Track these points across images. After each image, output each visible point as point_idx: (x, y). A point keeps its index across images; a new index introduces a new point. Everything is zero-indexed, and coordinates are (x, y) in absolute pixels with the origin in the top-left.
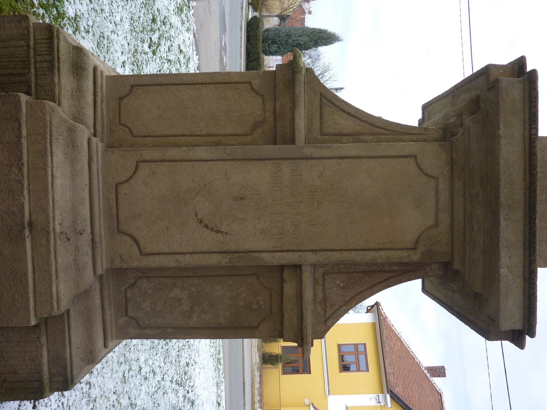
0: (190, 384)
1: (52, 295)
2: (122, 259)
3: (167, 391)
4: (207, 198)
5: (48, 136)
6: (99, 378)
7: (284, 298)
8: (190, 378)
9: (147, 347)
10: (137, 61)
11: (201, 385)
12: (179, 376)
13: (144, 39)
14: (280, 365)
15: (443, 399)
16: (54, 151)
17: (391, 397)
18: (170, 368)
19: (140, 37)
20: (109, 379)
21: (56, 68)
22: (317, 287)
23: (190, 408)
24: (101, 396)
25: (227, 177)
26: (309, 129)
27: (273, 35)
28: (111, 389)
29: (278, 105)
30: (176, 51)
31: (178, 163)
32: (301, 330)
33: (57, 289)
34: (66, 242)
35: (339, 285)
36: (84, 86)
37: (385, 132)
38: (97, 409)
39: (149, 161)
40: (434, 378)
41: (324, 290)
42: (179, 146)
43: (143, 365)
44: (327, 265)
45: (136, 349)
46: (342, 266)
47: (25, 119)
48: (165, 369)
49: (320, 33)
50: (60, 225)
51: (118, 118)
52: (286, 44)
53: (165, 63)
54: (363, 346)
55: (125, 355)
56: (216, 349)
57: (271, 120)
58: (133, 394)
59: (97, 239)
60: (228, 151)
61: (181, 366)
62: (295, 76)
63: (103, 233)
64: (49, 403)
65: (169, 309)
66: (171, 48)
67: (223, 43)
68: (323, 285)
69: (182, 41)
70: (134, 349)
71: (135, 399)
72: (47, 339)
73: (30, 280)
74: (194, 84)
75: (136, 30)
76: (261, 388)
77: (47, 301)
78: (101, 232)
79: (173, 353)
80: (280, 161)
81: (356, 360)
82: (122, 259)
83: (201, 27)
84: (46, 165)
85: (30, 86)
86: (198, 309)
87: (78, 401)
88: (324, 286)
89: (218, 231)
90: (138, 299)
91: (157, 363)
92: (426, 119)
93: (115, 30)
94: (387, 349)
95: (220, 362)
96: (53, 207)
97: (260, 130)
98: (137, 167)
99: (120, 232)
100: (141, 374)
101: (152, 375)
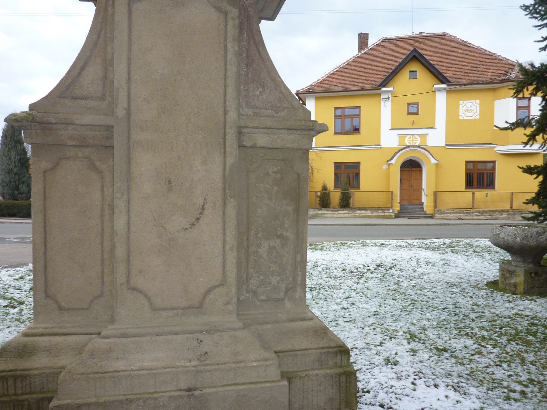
0: (362, 268)
1: (259, 366)
2: (228, 303)
3: (366, 286)
6: (348, 341)
7: (271, 147)
8: (356, 268)
9: (325, 304)
10: (29, 319)
11: (363, 258)
12: (353, 277)
14: (351, 191)
15: (388, 38)
16: (114, 369)
17: (384, 87)
20: (350, 333)
21: (23, 372)
22: (262, 115)
23: (383, 268)
24: (365, 339)
25: (146, 197)
27: (8, 189)
28: (359, 331)
29: (70, 142)
30: (20, 283)
34: (208, 356)
35: (261, 92)
38: (375, 342)
40: (369, 44)
42: (113, 249)
43: (341, 307)
45: (325, 313)
46: (242, 87)
47: (79, 400)
49: (6, 137)
50: (191, 361)
52: (19, 175)
54: (337, 110)
56: (333, 247)
57: (87, 151)
58: (365, 314)
61: (345, 275)
64: (366, 380)
66: (17, 287)
67: (16, 240)
69: (10, 278)
70: (325, 314)
71: (370, 312)
76: (371, 209)
79: (332, 282)
81: (350, 118)
82: (228, 303)
85: (43, 399)
87: (367, 357)
89: (203, 208)
90: (268, 288)
91: (340, 295)
94: (340, 87)
95: (345, 243)
96: (172, 368)
97: (98, 163)
98: (135, 289)
99: (201, 305)
100: (349, 308)
101: (350, 299)
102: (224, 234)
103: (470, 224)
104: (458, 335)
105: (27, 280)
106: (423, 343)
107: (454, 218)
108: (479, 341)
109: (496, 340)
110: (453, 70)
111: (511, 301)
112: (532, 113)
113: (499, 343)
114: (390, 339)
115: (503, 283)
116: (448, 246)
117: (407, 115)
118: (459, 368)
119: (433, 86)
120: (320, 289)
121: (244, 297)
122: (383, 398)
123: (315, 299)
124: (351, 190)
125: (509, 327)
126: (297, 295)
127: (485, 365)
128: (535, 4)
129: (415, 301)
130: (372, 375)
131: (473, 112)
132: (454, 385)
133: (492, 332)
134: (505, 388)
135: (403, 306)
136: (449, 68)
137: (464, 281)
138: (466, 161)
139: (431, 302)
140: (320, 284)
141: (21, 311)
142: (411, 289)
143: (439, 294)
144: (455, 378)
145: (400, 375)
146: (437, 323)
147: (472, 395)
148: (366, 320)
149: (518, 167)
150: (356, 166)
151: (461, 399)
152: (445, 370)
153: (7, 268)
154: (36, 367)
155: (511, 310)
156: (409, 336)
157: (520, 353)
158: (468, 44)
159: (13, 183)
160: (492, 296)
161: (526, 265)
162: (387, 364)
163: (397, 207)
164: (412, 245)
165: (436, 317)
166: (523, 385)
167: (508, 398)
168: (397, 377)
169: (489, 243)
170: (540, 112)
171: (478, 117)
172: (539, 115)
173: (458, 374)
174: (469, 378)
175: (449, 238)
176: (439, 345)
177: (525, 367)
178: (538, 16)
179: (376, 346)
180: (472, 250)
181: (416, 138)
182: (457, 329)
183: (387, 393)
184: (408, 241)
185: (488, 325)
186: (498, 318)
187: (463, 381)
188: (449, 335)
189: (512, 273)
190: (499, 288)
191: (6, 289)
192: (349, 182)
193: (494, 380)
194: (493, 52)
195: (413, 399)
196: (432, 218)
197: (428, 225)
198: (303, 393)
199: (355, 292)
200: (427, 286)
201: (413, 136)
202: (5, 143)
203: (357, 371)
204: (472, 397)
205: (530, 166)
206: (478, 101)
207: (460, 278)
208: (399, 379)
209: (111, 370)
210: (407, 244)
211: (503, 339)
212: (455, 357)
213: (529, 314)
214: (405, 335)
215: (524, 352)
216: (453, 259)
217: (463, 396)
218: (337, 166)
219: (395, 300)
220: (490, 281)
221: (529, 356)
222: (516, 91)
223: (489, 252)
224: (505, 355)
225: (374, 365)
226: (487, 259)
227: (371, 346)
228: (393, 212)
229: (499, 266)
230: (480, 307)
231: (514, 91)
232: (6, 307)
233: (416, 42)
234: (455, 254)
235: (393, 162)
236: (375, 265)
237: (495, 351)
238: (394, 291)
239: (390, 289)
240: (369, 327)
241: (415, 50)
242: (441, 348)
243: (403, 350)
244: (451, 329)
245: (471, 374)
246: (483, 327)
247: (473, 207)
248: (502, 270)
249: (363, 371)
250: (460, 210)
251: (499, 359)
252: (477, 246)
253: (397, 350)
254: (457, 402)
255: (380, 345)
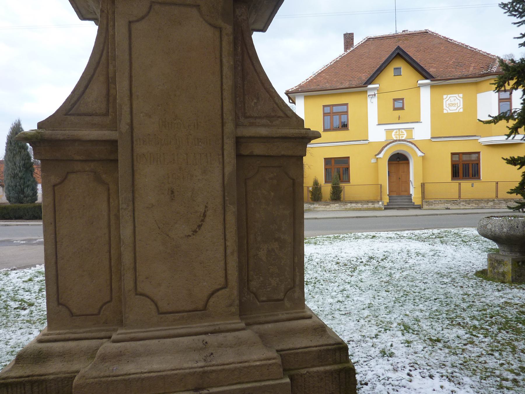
0: (355, 261)
2: (231, 305)
3: (360, 279)
4: (172, 226)
5: (110, 379)
6: (345, 334)
7: (266, 154)
9: (321, 297)
10: (40, 320)
11: (356, 251)
12: (347, 270)
13: (16, 315)
14: (342, 185)
15: (372, 37)
16: (125, 372)
17: (370, 84)
18: (340, 278)
19: (13, 319)
20: (346, 326)
21: (39, 378)
23: (376, 260)
24: (361, 331)
26: (102, 127)
27: (13, 193)
28: (355, 324)
29: (77, 157)
30: (29, 285)
31: (137, 255)
32: (295, 139)
33: (257, 361)
35: (255, 103)
36: (59, 350)
37: (105, 52)
38: (370, 334)
39: (136, 283)
41: (260, 118)
43: (336, 300)
44: (236, 114)
45: (321, 306)
46: (238, 99)
48: (340, 282)
49: (11, 143)
50: (197, 362)
51: (93, 316)
52: (24, 179)
53: (42, 295)
54: (325, 108)
55: (326, 314)
56: (326, 240)
58: (360, 307)
59: (211, 329)
60: (125, 206)
61: (339, 268)
62: (46, 139)
63: (206, 324)
64: (364, 372)
65: (277, 260)
66: (27, 289)
67: (22, 242)
68: (256, 118)
69: (19, 280)
70: (321, 307)
71: (365, 305)
72: (302, 368)
73: (249, 385)
74: (56, 242)
75: (5, 323)
76: (361, 202)
77: (268, 369)
78: (205, 326)
79: (327, 275)
80: (135, 155)
82: (231, 305)
83: (4, 264)
84: (139, 378)
86: (277, 234)
88: (256, 117)
89: (205, 215)
91: (335, 288)
92: (95, 16)
93: (5, 342)
94: (328, 86)
95: (337, 237)
96: (180, 369)
98: (141, 294)
99: (205, 308)
100: (344, 301)
101: (345, 292)
102: (225, 240)
103: (458, 214)
104: (450, 325)
105: (35, 282)
106: (417, 334)
107: (441, 208)
108: (471, 331)
109: (487, 329)
110: (436, 66)
111: (500, 289)
112: (514, 107)
113: (490, 332)
114: (385, 331)
115: (492, 272)
116: (437, 236)
117: (393, 110)
118: (452, 358)
119: (417, 82)
120: (315, 283)
121: (245, 299)
122: (380, 390)
123: (311, 293)
124: (341, 184)
125: (499, 316)
126: (296, 295)
127: (478, 354)
128: (513, 2)
129: (407, 292)
130: (369, 367)
131: (456, 105)
132: (448, 375)
133: (482, 321)
134: (498, 377)
135: (396, 298)
136: (432, 64)
137: (454, 271)
138: (451, 153)
139: (423, 293)
140: (315, 278)
141: (32, 312)
142: (403, 281)
143: (430, 285)
144: (449, 368)
145: (396, 367)
146: (430, 314)
147: (466, 385)
148: (361, 313)
149: (503, 158)
150: (345, 160)
151: (456, 389)
152: (439, 360)
153: (16, 270)
154: (51, 372)
155: (501, 299)
156: (403, 328)
157: (511, 341)
158: (449, 41)
159: (18, 187)
160: (482, 286)
161: (513, 254)
162: (383, 356)
163: (386, 200)
164: (402, 236)
165: (428, 308)
166: (515, 373)
167: (501, 387)
168: (394, 368)
169: (476, 233)
170: (522, 105)
171: (461, 110)
172: (521, 108)
173: (452, 365)
174: (463, 368)
175: (438, 228)
176: (433, 336)
177: (516, 355)
178: (517, 13)
179: (372, 338)
180: (461, 239)
181: (402, 132)
182: (449, 319)
183: (384, 384)
184: (398, 233)
185: (479, 315)
186: (488, 307)
187: (457, 370)
188: (441, 325)
189: (500, 262)
190: (488, 277)
191: (16, 292)
192: (340, 176)
193: (486, 369)
194: (474, 48)
195: (410, 390)
196: (421, 209)
197: (417, 216)
198: (305, 389)
199: (349, 285)
200: (419, 277)
201: (399, 130)
202: (10, 149)
203: (354, 363)
204: (466, 386)
205: (514, 157)
206: (461, 95)
207: (450, 268)
208: (395, 370)
209: (122, 373)
210: (397, 236)
211: (494, 327)
212: (449, 347)
213: (518, 302)
214: (400, 327)
215: (514, 340)
216: (442, 249)
217: (457, 386)
218: (328, 161)
219: (389, 292)
220: (479, 270)
221: (519, 345)
222: (497, 85)
223: (477, 242)
224: (496, 344)
225: (371, 358)
226: (475, 248)
227: (367, 338)
228: (383, 204)
229: (487, 256)
230: (471, 296)
231: (496, 86)
232: (17, 309)
233: (399, 40)
234: (444, 245)
235: (381, 156)
236: (367, 258)
237: (486, 340)
238: (386, 282)
239: (382, 281)
240: (364, 319)
241: (399, 48)
242: (435, 338)
243: (397, 341)
244: (444, 319)
245: (465, 364)
246: (474, 316)
247: (460, 197)
248: (490, 259)
249: (360, 363)
250: (447, 201)
251: (490, 348)
252: (465, 236)
253: (392, 342)
254: (452, 392)
255: (376, 337)
